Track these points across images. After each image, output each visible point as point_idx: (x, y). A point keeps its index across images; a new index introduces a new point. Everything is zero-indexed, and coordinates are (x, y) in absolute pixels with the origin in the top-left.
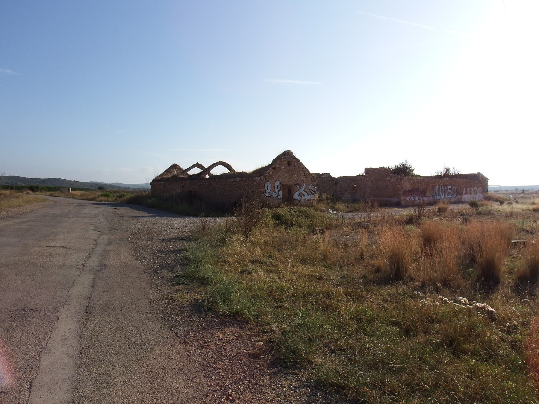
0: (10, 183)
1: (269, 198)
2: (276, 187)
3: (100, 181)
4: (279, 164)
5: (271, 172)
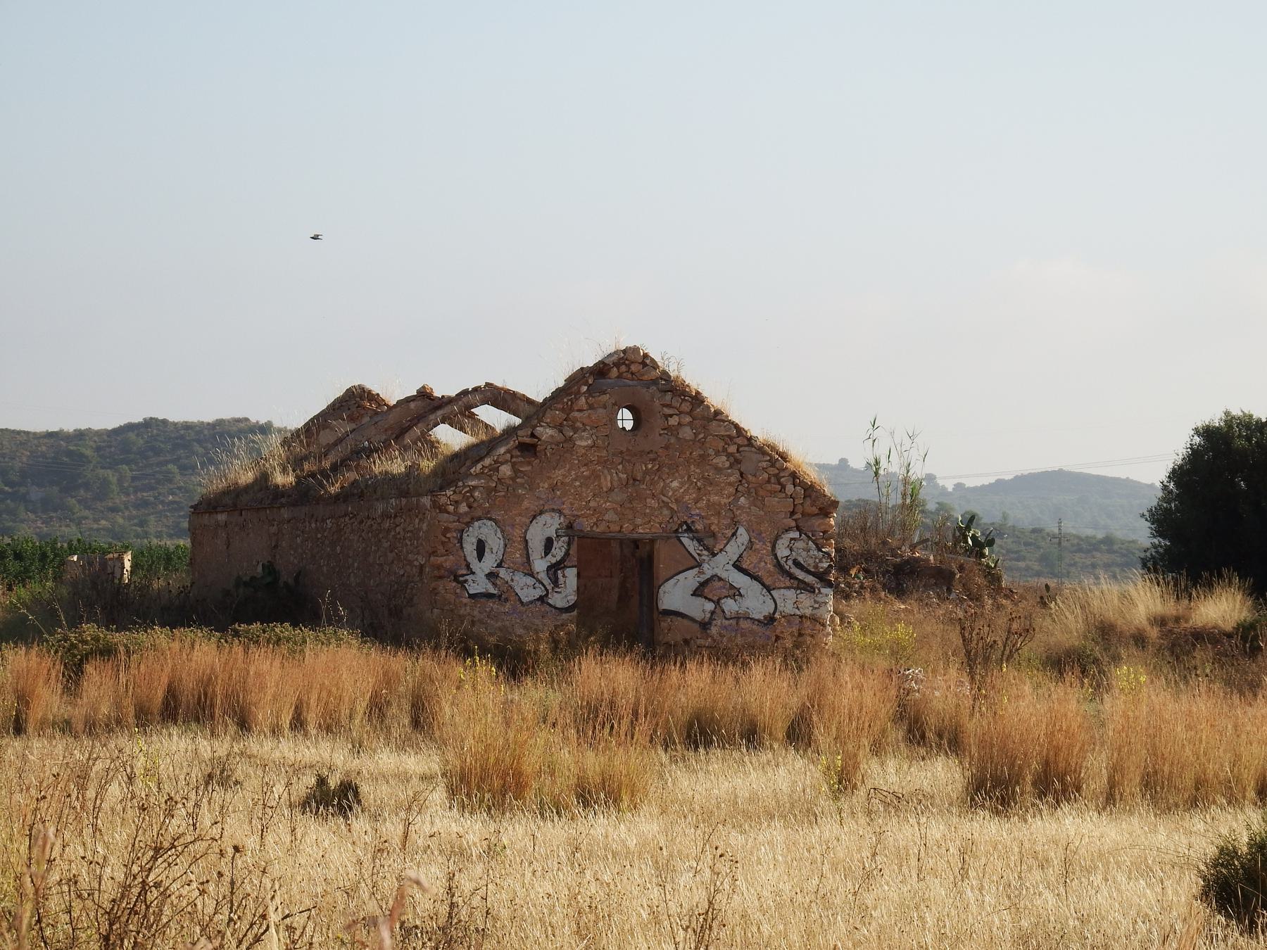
2: (536, 545)
4: (560, 428)
5: (506, 470)
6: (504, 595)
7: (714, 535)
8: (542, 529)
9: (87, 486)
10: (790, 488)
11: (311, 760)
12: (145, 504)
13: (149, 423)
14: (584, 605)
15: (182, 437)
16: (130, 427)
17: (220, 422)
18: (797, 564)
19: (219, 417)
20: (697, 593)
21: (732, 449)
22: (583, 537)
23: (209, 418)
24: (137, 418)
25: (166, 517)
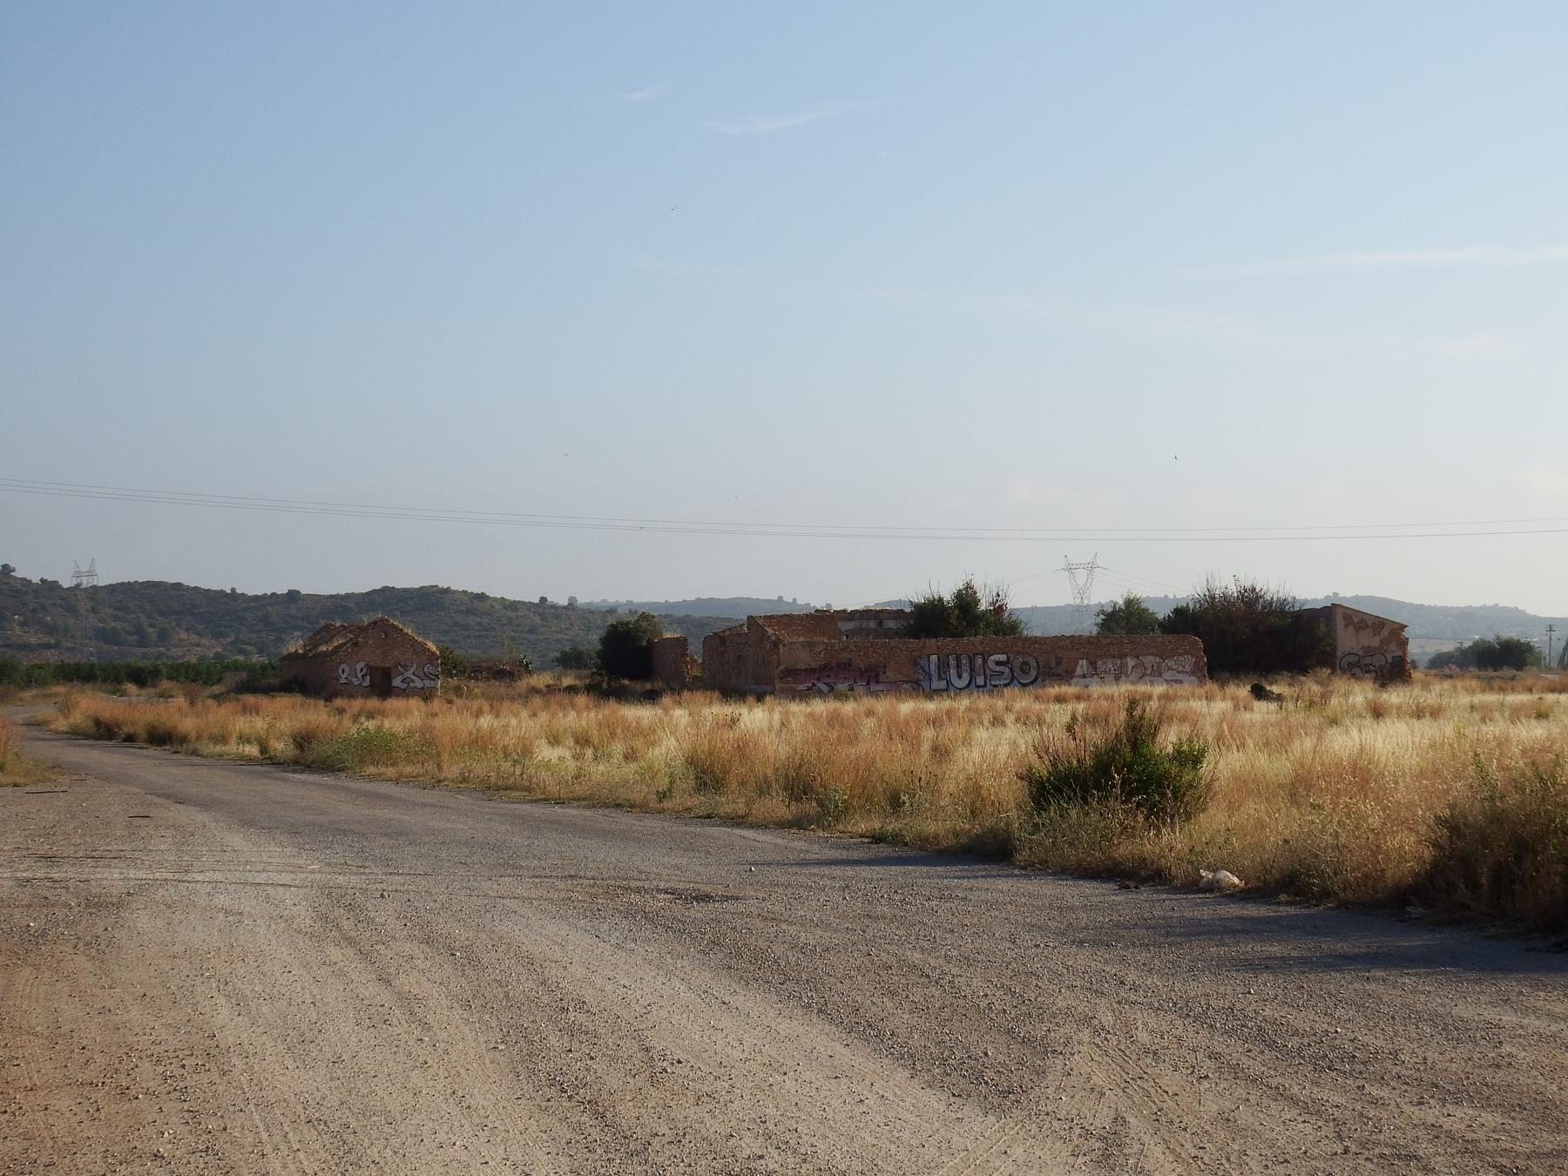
0: (128, 633)
1: (347, 686)
5: (350, 650)
8: (362, 664)
13: (385, 589)
14: (372, 685)
15: (402, 596)
16: (375, 591)
19: (422, 585)
20: (402, 682)
23: (417, 586)
24: (379, 587)
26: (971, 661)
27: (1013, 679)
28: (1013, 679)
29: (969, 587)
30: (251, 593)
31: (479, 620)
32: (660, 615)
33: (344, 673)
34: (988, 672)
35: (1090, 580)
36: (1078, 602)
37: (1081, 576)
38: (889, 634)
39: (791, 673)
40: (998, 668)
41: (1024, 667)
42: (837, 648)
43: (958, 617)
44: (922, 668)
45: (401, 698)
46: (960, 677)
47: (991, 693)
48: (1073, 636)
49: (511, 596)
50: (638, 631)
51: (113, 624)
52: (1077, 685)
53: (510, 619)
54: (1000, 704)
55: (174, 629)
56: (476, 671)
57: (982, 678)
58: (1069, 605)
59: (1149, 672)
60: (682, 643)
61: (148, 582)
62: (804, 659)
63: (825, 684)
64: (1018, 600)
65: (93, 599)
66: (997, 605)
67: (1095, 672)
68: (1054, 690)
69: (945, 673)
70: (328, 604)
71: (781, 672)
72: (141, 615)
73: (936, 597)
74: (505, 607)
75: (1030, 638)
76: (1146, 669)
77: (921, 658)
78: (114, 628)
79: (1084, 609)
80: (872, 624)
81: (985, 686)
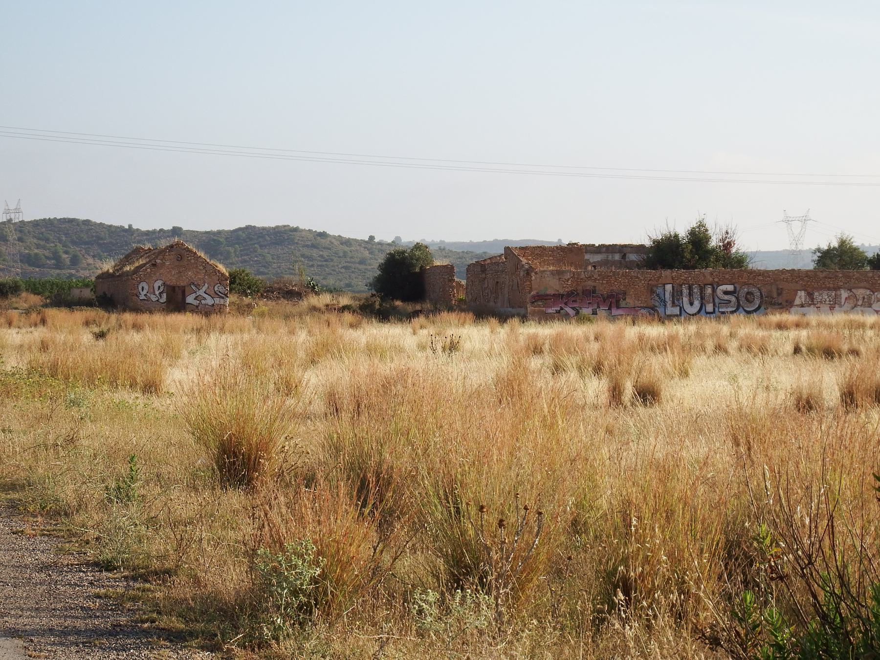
0: (48, 258)
1: (145, 302)
3: (466, 240)
4: (162, 260)
5: (149, 270)
6: (148, 300)
7: (199, 285)
9: (221, 254)
10: (218, 274)
11: (617, 411)
12: (245, 261)
15: (262, 233)
16: (240, 229)
17: (277, 227)
18: (220, 292)
21: (204, 265)
22: (168, 286)
23: (273, 225)
24: (243, 226)
25: (253, 266)
26: (702, 290)
27: (738, 306)
28: (738, 306)
29: (701, 225)
30: (144, 228)
31: (321, 253)
32: (463, 252)
33: (144, 290)
34: (717, 300)
35: (804, 230)
36: (793, 248)
37: (796, 226)
38: (630, 265)
39: (542, 298)
40: (726, 297)
41: (749, 296)
42: (583, 276)
43: (691, 251)
44: (658, 295)
45: (63, 309)
46: (691, 304)
47: (718, 319)
48: (793, 270)
49: (347, 235)
50: (412, 259)
51: (36, 251)
52: (796, 313)
53: (345, 252)
54: (725, 329)
55: (83, 256)
56: (268, 291)
57: (711, 305)
58: (786, 250)
59: (860, 303)
60: (449, 270)
61: (64, 219)
62: (553, 285)
63: (571, 308)
64: (743, 245)
65: (21, 231)
66: (726, 242)
67: (811, 301)
68: (776, 317)
69: (678, 300)
70: (204, 238)
71: (534, 297)
72: (58, 244)
73: (672, 234)
74: (342, 244)
75: (755, 271)
76: (857, 300)
77: (657, 286)
78: (36, 254)
79: (798, 253)
80: (617, 257)
81: (714, 312)
